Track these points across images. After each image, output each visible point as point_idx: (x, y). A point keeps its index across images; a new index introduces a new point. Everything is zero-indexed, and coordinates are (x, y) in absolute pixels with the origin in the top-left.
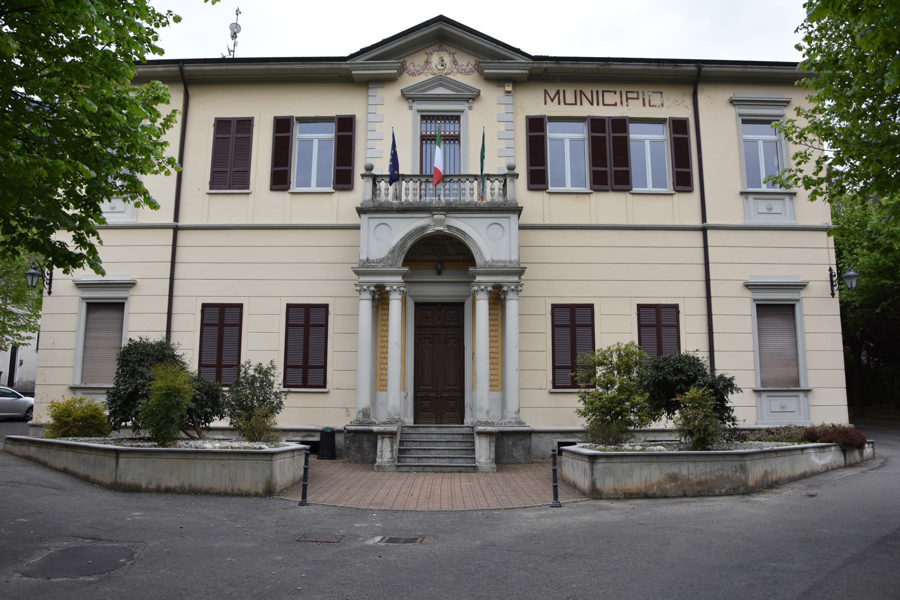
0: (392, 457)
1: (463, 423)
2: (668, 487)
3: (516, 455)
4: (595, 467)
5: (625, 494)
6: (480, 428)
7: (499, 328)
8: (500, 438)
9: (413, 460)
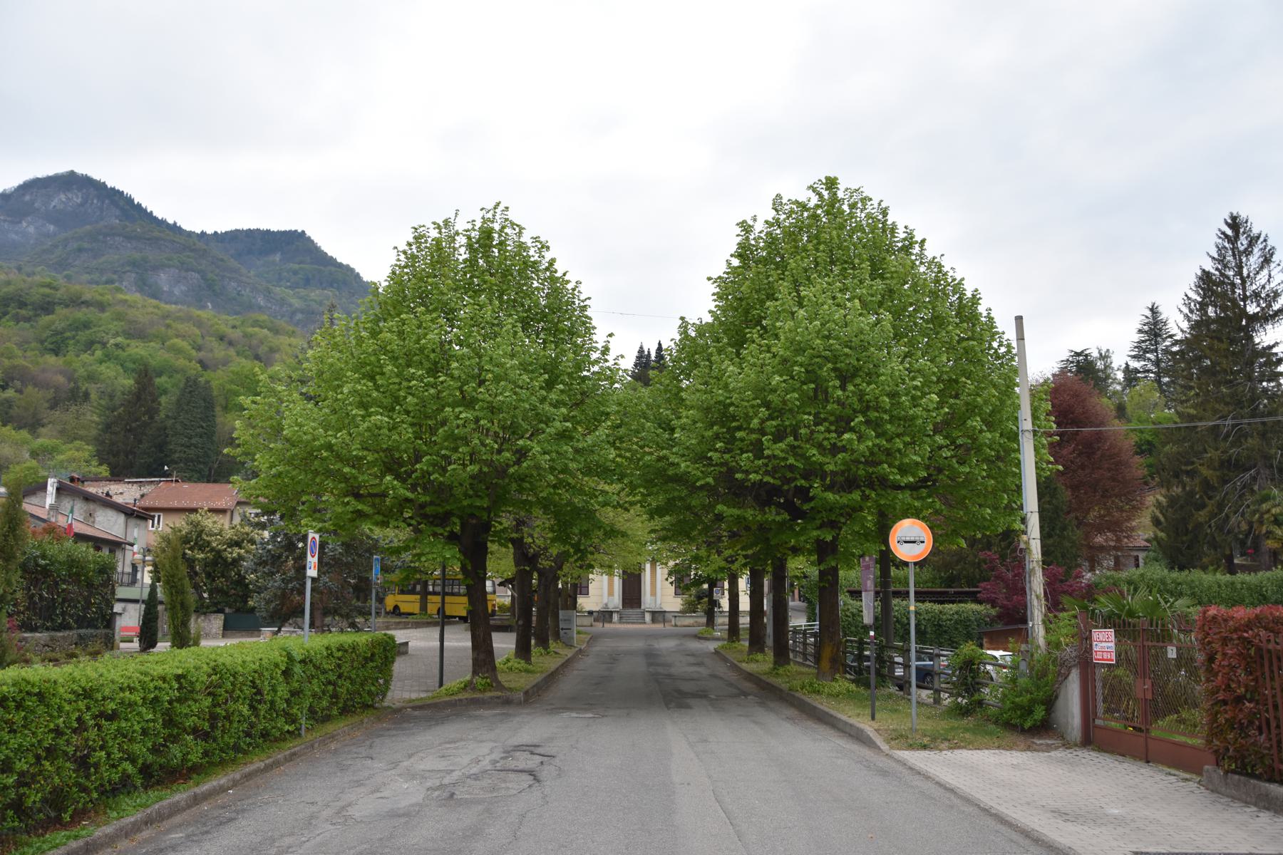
8: (653, 613)
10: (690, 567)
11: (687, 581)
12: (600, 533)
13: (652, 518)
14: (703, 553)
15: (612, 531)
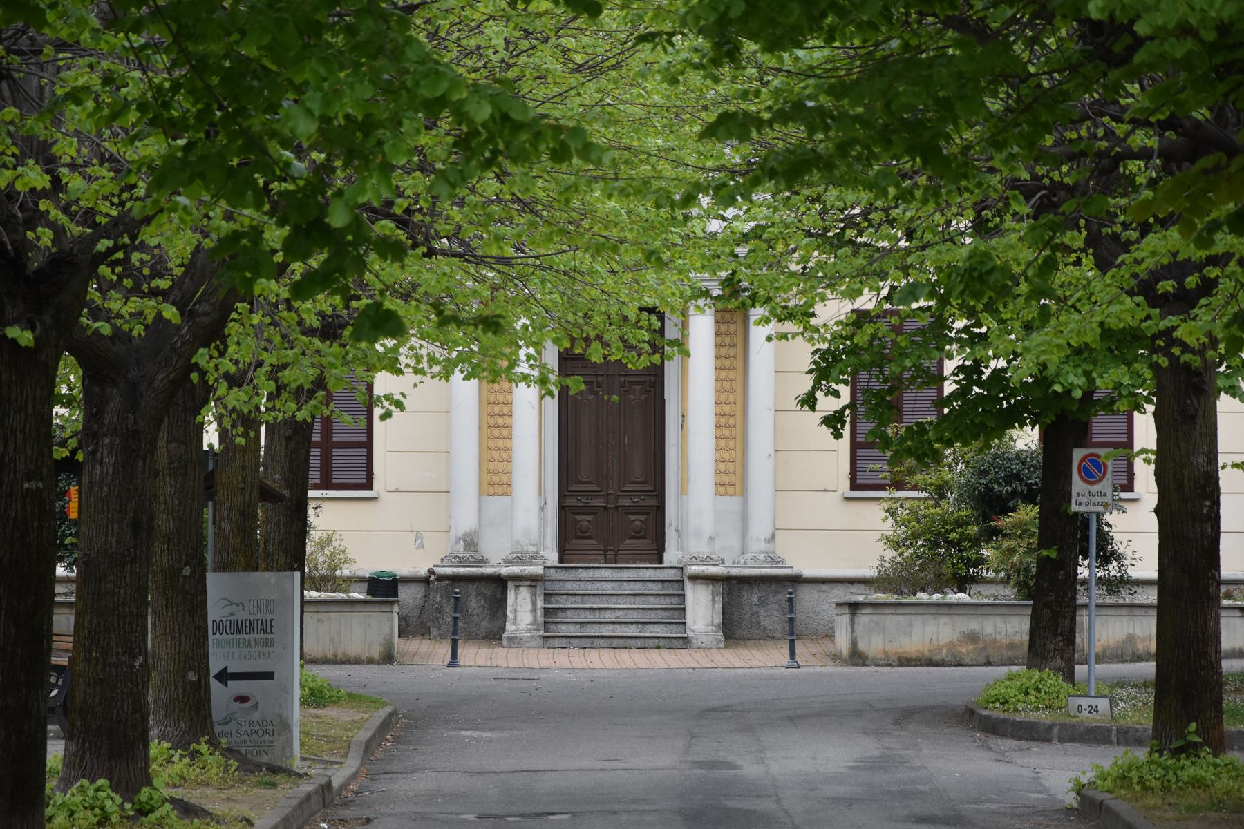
0: (535, 622)
1: (661, 562)
2: (964, 650)
3: (765, 622)
4: (856, 620)
5: (900, 659)
6: (695, 569)
7: (738, 363)
8: (732, 587)
9: (571, 627)
10: (937, 329)
11: (918, 409)
12: (436, 141)
13: (725, 52)
14: (1015, 247)
15: (503, 119)
